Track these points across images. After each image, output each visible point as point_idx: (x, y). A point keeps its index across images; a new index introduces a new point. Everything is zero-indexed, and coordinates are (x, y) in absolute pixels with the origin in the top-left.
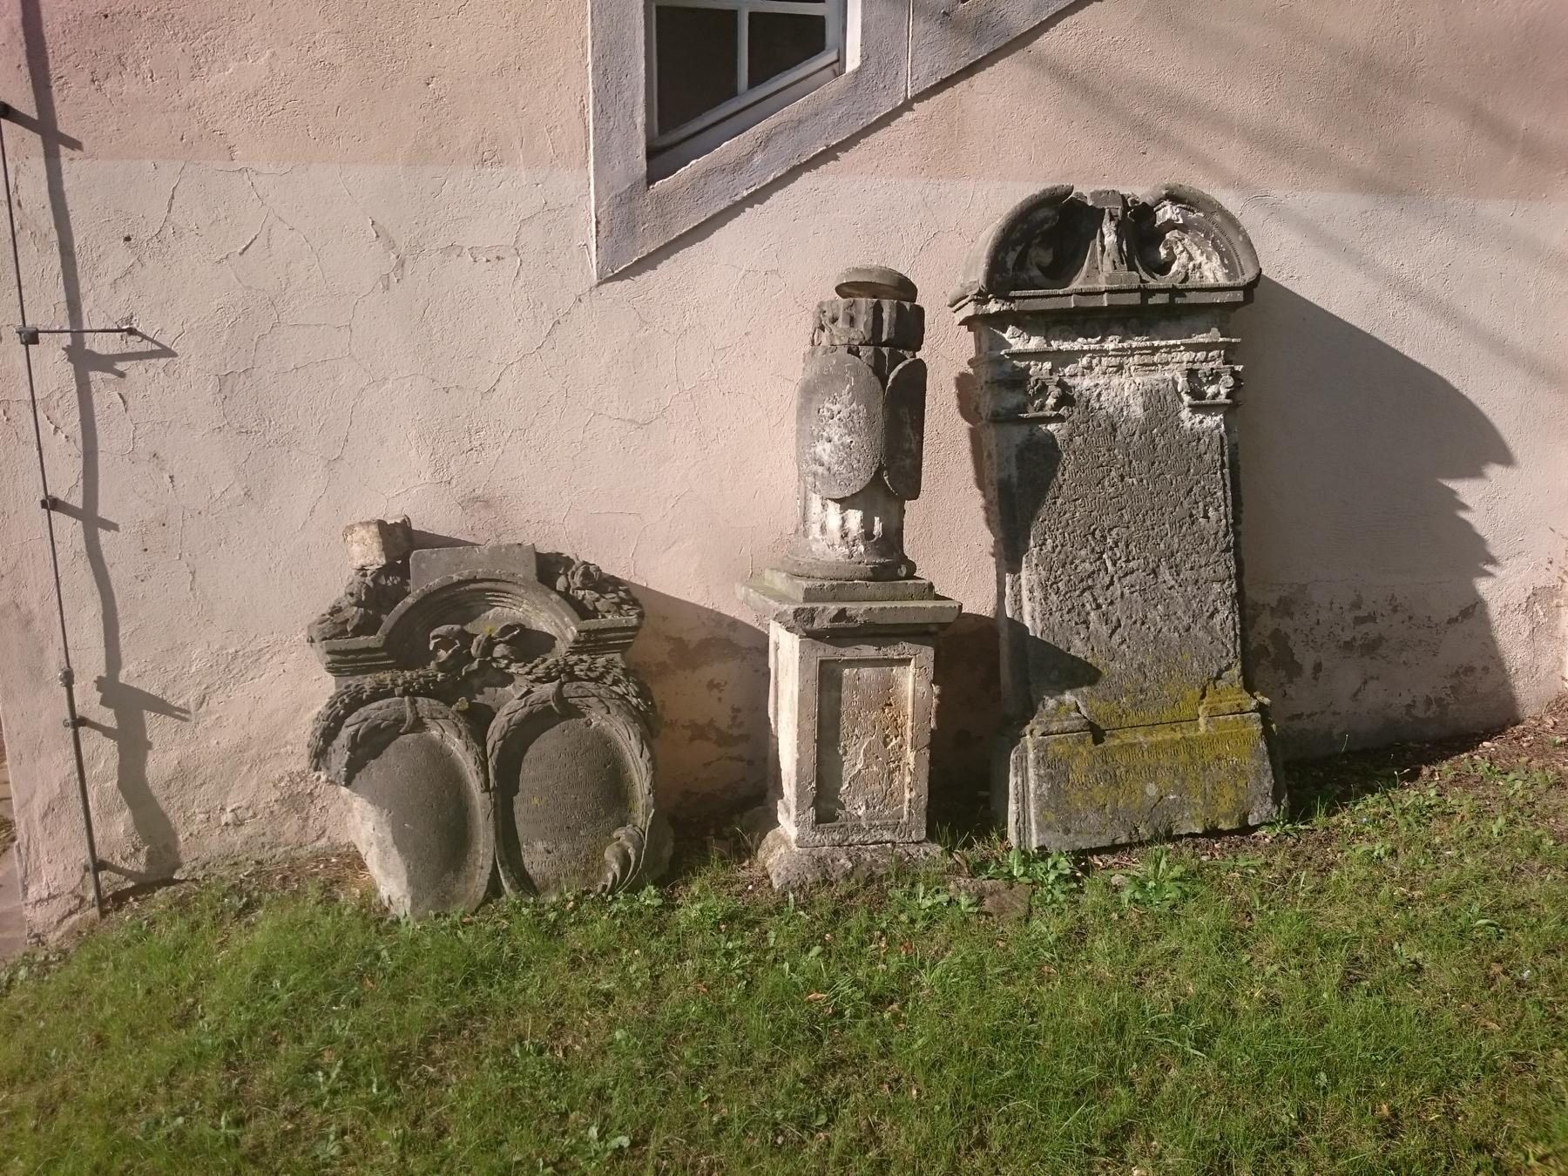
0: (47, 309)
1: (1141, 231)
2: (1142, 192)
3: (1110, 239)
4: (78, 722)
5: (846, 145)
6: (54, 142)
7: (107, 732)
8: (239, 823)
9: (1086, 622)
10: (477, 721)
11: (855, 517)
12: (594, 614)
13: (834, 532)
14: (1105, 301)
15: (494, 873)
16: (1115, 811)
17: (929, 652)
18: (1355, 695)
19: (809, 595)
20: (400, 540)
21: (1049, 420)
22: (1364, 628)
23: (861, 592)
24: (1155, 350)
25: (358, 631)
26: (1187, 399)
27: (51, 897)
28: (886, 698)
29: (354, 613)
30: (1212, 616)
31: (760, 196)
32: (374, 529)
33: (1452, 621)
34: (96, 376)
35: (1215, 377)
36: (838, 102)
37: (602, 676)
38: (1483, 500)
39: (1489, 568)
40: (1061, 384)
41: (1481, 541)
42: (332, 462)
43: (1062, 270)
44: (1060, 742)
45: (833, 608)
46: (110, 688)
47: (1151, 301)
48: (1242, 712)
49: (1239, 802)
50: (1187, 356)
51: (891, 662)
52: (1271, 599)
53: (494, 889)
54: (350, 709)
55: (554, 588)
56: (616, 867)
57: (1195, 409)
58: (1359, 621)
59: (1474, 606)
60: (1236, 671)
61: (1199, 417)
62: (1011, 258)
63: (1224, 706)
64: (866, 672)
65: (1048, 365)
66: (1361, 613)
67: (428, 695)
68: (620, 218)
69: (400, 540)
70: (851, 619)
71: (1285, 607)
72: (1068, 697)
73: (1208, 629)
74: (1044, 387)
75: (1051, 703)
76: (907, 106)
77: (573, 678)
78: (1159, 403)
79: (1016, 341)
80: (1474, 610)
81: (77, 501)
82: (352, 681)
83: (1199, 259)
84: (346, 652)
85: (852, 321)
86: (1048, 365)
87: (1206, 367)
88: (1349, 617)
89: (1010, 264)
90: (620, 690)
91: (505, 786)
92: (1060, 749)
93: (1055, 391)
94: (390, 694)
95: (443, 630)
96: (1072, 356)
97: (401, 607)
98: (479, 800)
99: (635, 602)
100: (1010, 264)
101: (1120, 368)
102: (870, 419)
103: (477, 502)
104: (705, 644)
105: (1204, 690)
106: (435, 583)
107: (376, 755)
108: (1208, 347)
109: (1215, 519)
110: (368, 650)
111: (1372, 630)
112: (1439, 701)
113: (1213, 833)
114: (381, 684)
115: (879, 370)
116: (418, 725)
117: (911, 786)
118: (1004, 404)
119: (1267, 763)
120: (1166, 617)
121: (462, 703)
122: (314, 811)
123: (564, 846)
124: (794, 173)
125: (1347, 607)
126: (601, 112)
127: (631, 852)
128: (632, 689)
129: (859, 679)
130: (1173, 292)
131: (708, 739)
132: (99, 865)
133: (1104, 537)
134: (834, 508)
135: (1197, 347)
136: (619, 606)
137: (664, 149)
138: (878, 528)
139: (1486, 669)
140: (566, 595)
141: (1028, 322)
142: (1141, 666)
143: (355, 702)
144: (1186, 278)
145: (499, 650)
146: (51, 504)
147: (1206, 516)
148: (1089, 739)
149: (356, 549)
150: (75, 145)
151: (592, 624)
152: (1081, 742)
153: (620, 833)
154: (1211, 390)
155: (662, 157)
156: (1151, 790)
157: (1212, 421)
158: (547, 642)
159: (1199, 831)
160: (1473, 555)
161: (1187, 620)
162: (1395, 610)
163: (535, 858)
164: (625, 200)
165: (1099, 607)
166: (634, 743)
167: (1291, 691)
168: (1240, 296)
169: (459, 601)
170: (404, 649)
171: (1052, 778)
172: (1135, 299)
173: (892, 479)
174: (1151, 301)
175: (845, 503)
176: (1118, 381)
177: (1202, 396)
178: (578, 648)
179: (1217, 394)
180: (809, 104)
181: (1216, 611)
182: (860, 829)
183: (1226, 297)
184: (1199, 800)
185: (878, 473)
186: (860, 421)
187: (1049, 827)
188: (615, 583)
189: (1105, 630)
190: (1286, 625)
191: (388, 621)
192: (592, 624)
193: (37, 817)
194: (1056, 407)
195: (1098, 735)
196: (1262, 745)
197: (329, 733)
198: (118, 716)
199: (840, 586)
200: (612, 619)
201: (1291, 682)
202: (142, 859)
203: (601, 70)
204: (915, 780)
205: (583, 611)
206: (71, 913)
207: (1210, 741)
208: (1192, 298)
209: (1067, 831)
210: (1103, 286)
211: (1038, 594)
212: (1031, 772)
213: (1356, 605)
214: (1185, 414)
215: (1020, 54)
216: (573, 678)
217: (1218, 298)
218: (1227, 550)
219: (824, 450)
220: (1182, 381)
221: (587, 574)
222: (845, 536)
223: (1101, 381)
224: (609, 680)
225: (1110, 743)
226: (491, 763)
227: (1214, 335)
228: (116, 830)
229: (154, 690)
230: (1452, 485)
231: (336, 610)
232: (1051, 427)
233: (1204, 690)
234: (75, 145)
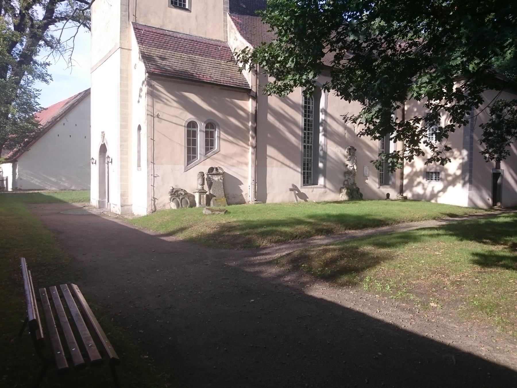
0: (153, 174)
1: (217, 169)
2: (217, 167)
6: (154, 164)
13: (200, 187)
38: (241, 187)
43: (212, 172)
68: (185, 168)
80: (242, 195)
91: (181, 202)
103: (176, 186)
117: (205, 203)
118: (209, 179)
160: (242, 191)
169: (177, 191)
173: (203, 184)
176: (216, 178)
199: (200, 190)
228: (153, 207)
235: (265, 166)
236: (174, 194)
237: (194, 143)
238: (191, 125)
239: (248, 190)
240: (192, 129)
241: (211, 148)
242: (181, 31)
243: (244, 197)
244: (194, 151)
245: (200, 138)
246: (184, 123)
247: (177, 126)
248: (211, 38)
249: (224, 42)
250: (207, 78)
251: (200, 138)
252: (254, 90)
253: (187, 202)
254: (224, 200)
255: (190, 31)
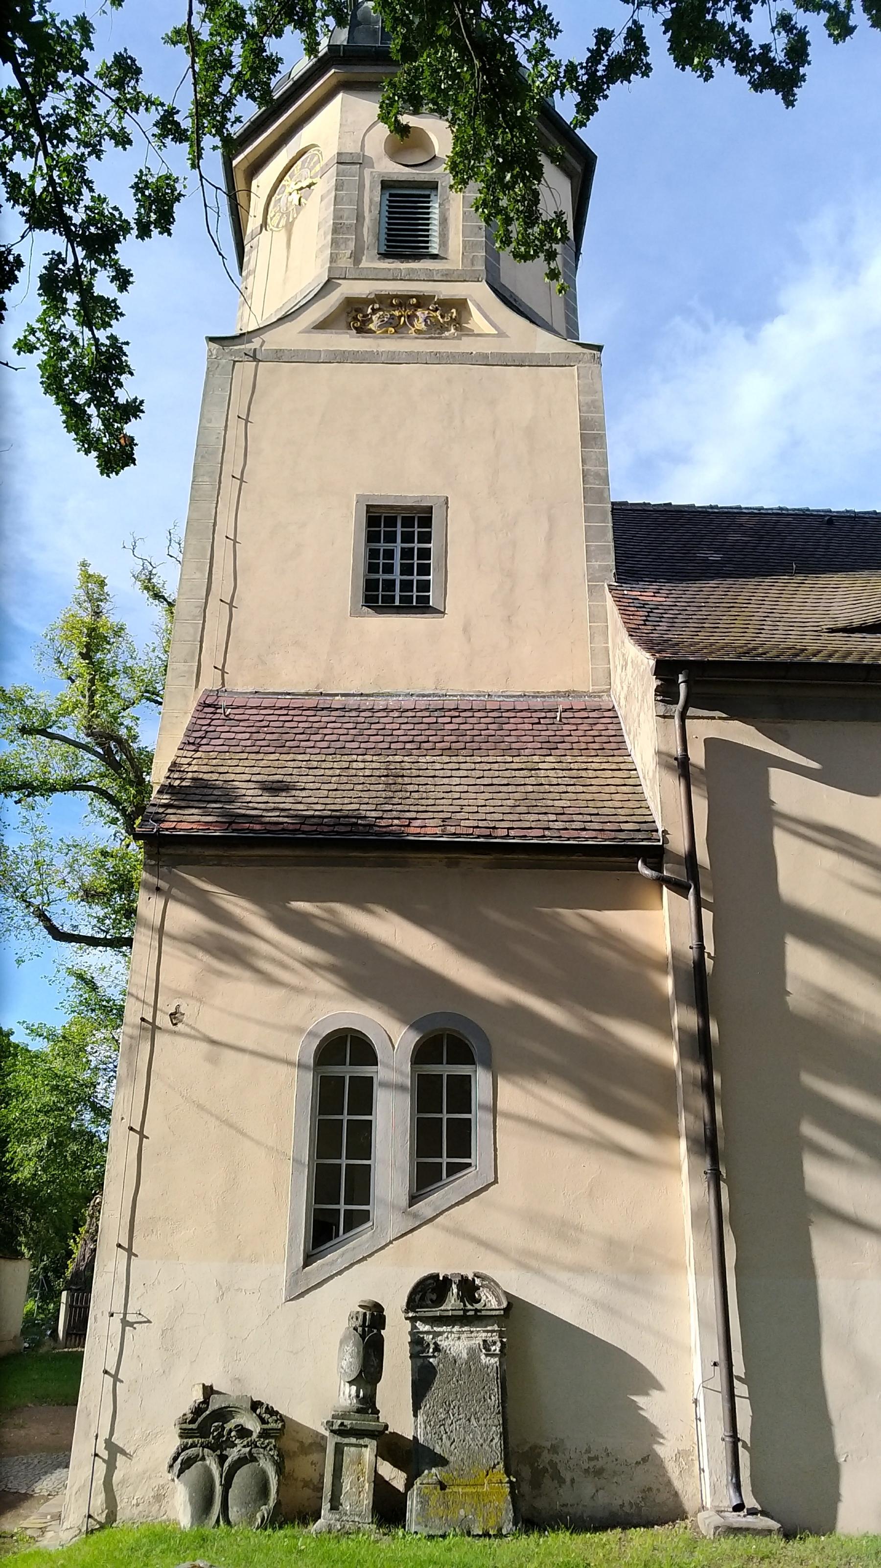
0: (118, 1307)
3: (455, 1291)
4: (96, 1455)
5: (370, 1255)
6: (130, 1253)
7: (104, 1460)
8: (138, 1505)
9: (441, 1439)
10: (222, 1459)
11: (354, 1388)
12: (268, 1423)
13: (346, 1396)
14: (450, 1313)
15: (219, 1517)
16: (446, 1519)
17: (375, 1442)
18: (593, 1497)
19: (334, 1417)
20: (209, 1391)
21: (430, 1357)
22: (593, 1463)
23: (352, 1417)
24: (472, 1332)
25: (190, 1423)
26: (484, 1351)
27: (71, 1528)
28: (359, 1461)
29: (190, 1416)
30: (492, 1441)
31: (340, 1273)
32: (201, 1386)
33: (638, 1463)
34: (127, 1328)
35: (494, 1343)
36: (367, 1242)
37: (266, 1447)
38: (651, 1405)
39: (661, 1441)
40: (435, 1343)
41: (656, 1427)
42: (191, 1362)
44: (427, 1488)
45: (339, 1422)
46: (110, 1445)
47: (468, 1314)
48: (501, 1483)
49: (498, 1522)
50: (484, 1334)
51: (361, 1446)
52: (548, 1445)
53: (218, 1521)
54: (183, 1450)
55: (255, 1412)
56: (259, 1521)
57: (487, 1355)
58: (590, 1459)
59: (648, 1456)
60: (501, 1465)
61: (489, 1358)
62: (418, 1297)
63: (494, 1480)
64: (353, 1449)
65: (431, 1336)
66: (592, 1455)
67: (208, 1448)
68: (294, 1278)
69: (209, 1391)
70: (346, 1426)
71: (554, 1449)
72: (434, 1470)
73: (491, 1447)
74: (428, 1345)
75: (426, 1472)
76: (391, 1242)
77: (256, 1446)
78: (473, 1353)
79: (422, 1327)
81: (113, 1372)
82: (185, 1440)
83: (490, 1298)
84: (185, 1429)
85: (357, 1319)
86: (431, 1336)
87: (491, 1339)
88: (585, 1457)
89: (417, 1300)
90: (271, 1453)
92: (426, 1491)
93: (432, 1346)
94: (196, 1446)
95: (216, 1424)
96: (440, 1334)
97: (204, 1415)
98: (218, 1489)
99: (282, 1421)
100: (417, 1300)
101: (459, 1338)
102: (358, 1352)
104: (311, 1444)
105: (488, 1472)
106: (216, 1407)
107: (189, 1468)
108: (492, 1331)
109: (494, 1400)
110: (192, 1429)
111: (599, 1464)
112: (637, 1505)
113: (486, 1535)
114: (194, 1442)
115: (363, 1336)
116: (203, 1459)
119: (511, 1506)
120: (473, 1439)
121: (218, 1452)
122: (164, 1503)
123: (243, 1510)
124: (352, 1265)
125: (583, 1451)
126: (290, 1246)
127: (266, 1516)
128: (276, 1453)
129: (350, 1452)
130: (476, 1310)
131: (309, 1488)
132: (90, 1516)
133: (450, 1405)
134: (347, 1385)
135: (488, 1331)
136: (276, 1421)
137: (416, 1197)
138: (361, 1394)
139: (658, 1490)
140: (259, 1416)
141: (425, 1320)
142: (462, 1460)
143: (185, 1448)
144: (485, 1305)
145: (233, 1434)
146: (106, 1372)
147: (490, 1398)
148: (439, 1487)
149: (194, 1393)
150: (136, 1256)
151: (265, 1426)
152: (436, 1488)
153: (263, 1507)
154: (493, 1348)
155: (309, 1259)
156: (462, 1512)
157: (494, 1361)
158: (249, 1433)
159: (481, 1533)
160: (653, 1433)
161: (481, 1441)
162: (608, 1454)
163: (233, 1514)
164: (296, 1273)
165: (446, 1433)
166: (273, 1473)
167: (561, 1491)
168: (502, 1312)
169: (224, 1414)
170: (203, 1431)
171: (422, 1502)
172: (461, 1313)
174: (468, 1314)
175: (351, 1383)
176: (458, 1343)
177: (490, 1350)
178: (260, 1436)
179: (495, 1350)
180: (361, 1240)
181: (493, 1439)
182: (346, 1514)
183: (497, 1313)
184: (481, 1519)
185: (361, 1372)
186: (355, 1354)
187: (419, 1524)
188: (277, 1413)
189: (448, 1443)
190: (556, 1458)
191: (200, 1419)
192: (265, 1426)
193: (74, 1493)
194: (433, 1352)
195: (443, 1487)
196: (509, 1498)
197: (175, 1459)
198: (109, 1454)
199: (344, 1415)
200: (272, 1425)
201: (560, 1486)
202: (104, 1515)
203: (291, 1232)
204: (368, 1496)
205: (263, 1421)
206: (76, 1536)
207: (487, 1494)
208: (483, 1313)
209: (426, 1526)
210: (449, 1308)
211: (423, 1426)
212: (415, 1502)
213: (588, 1451)
214: (483, 1357)
215: (431, 1224)
216: (256, 1446)
217: (494, 1313)
218: (499, 1413)
219: (344, 1364)
220: (481, 1343)
221: (267, 1408)
222: (350, 1396)
223: (452, 1343)
224: (268, 1448)
225: (447, 1490)
226: (224, 1474)
227: (496, 1328)
228: (99, 1500)
229: (121, 1445)
230: (634, 1398)
231: (185, 1415)
232: (431, 1360)
233: (488, 1472)
234: (136, 1256)
235: (807, 1270)
236: (203, 1431)
237: (362, 1140)
238: (342, 1051)
239: (688, 1423)
240: (348, 1071)
241: (454, 1169)
242: (402, 688)
243: (673, 1471)
244: (360, 1184)
245: (392, 1120)
246: (302, 1049)
247: (264, 1062)
248: (530, 689)
249: (597, 695)
250: (428, 828)
251: (392, 1120)
252: (679, 844)
253: (263, 1491)
254: (497, 1490)
255: (438, 681)
